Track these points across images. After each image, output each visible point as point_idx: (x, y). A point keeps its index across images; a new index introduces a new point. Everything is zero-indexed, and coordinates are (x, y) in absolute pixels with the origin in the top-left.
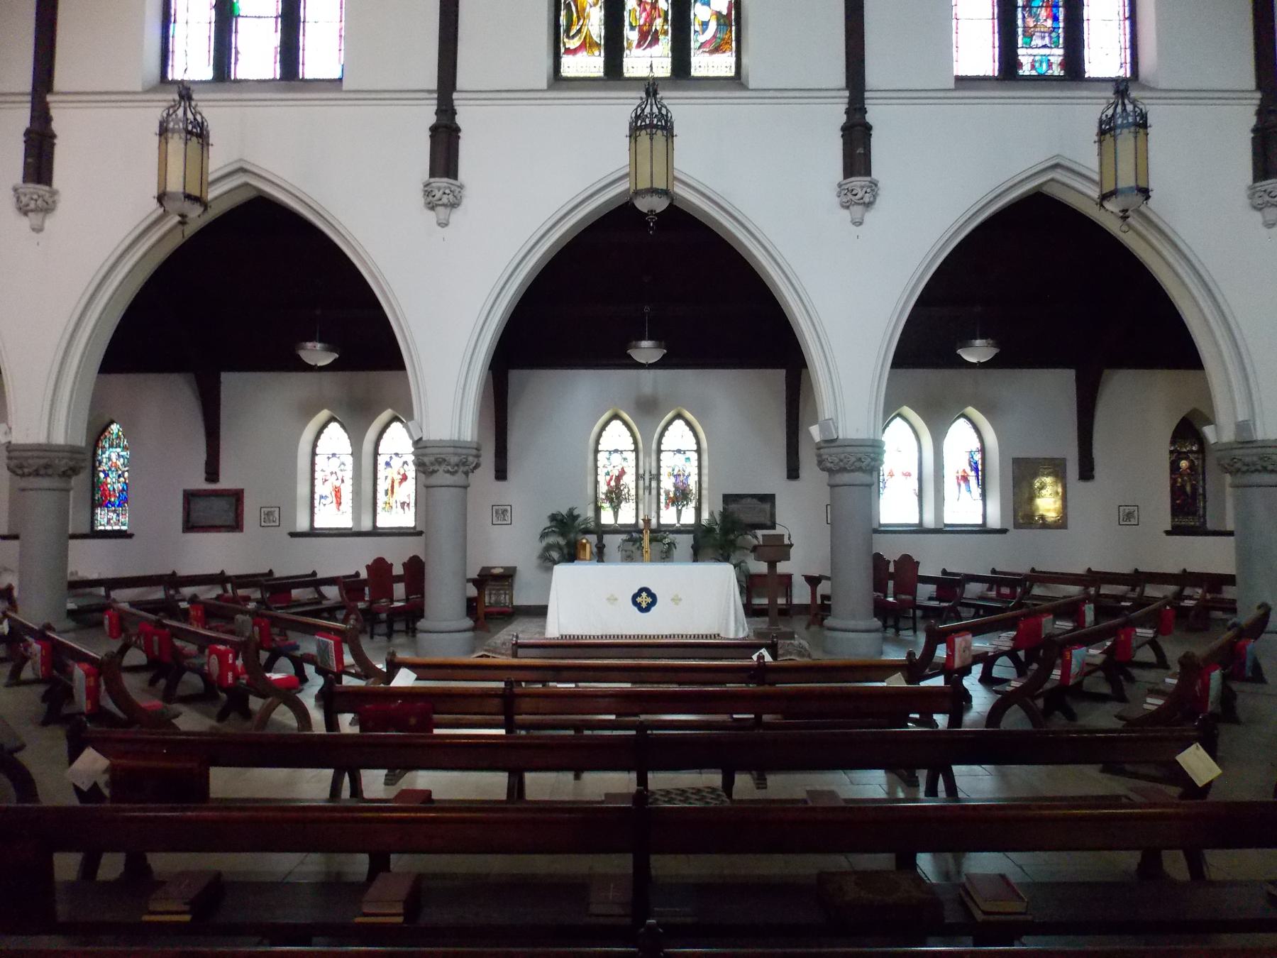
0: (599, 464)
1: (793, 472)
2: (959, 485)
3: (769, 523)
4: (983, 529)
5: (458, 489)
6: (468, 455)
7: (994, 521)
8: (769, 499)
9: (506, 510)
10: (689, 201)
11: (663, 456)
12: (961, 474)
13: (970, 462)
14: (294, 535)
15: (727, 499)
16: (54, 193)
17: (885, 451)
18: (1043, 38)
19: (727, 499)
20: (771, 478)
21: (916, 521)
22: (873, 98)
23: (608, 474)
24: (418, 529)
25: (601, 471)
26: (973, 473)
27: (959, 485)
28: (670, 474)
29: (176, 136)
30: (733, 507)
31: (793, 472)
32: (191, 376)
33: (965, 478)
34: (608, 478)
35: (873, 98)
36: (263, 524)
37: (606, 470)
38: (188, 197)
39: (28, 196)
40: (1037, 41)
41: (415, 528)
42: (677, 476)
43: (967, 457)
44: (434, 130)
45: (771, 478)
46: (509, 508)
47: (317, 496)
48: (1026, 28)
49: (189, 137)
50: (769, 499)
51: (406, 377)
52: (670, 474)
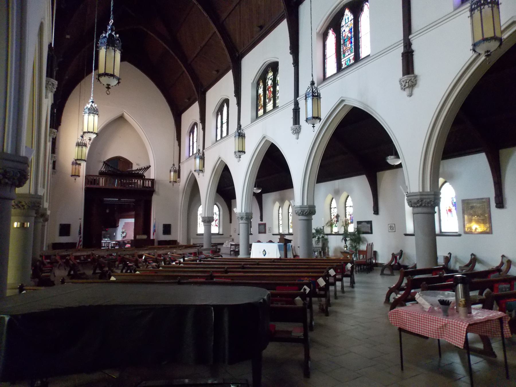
0: (332, 212)
1: (376, 211)
2: (447, 213)
3: (370, 231)
4: (218, 234)
5: (420, 215)
6: (243, 216)
7: (221, 233)
8: (370, 223)
9: (390, 226)
10: (9, 241)
11: (347, 208)
12: (448, 208)
13: (452, 203)
14: (406, 235)
15: (359, 223)
16: (416, 77)
17: (440, 198)
18: (348, 52)
19: (359, 223)
20: (369, 216)
21: (218, 232)
22: (299, 99)
23: (334, 215)
24: (459, 233)
25: (332, 215)
26: (454, 208)
27: (447, 213)
28: (349, 215)
29: (309, 98)
30: (359, 226)
31: (376, 211)
32: (120, 220)
33: (450, 210)
34: (334, 217)
35: (299, 99)
36: (390, 231)
37: (333, 214)
38: (239, 151)
39: (405, 82)
40: (347, 54)
41: (338, 232)
42: (351, 215)
43: (451, 200)
44: (403, 54)
45: (369, 216)
46: (389, 225)
47: (280, 225)
48: (343, 51)
49: (313, 97)
50: (370, 223)
51: (403, 171)
52: (349, 215)
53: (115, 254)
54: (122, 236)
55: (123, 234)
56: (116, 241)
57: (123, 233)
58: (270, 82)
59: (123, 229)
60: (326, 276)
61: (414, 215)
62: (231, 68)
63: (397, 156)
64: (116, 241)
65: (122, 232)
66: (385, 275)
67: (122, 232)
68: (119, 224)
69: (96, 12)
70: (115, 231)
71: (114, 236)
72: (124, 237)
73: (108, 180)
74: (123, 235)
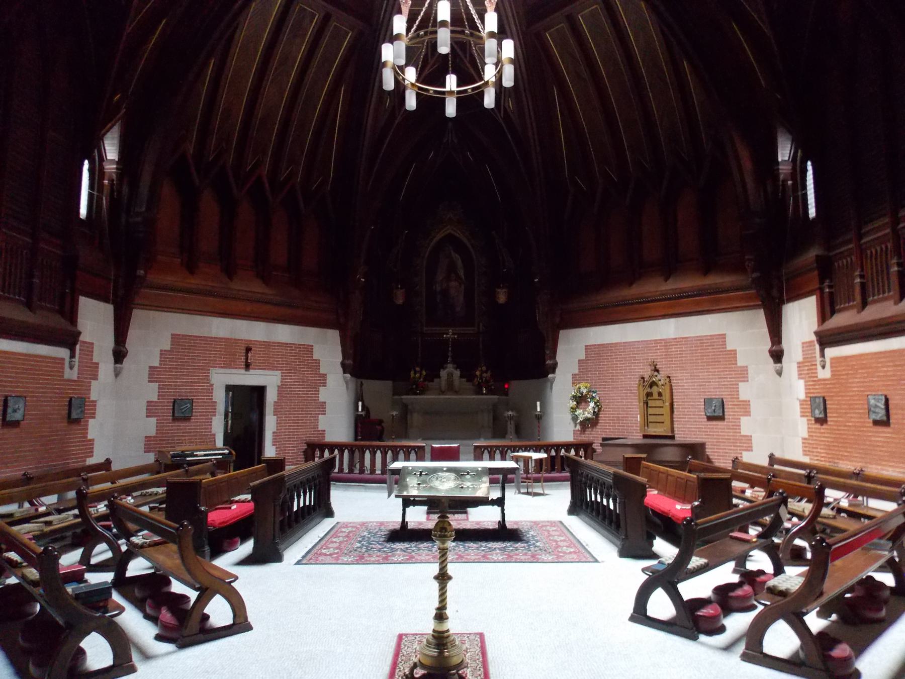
32: (563, 333)
53: (120, 542)
54: (575, 418)
55: (578, 404)
56: (547, 448)
57: (580, 400)
58: (831, 386)
59: (576, 379)
60: (113, 497)
61: (478, 638)
62: (826, 253)
63: (806, 502)
64: (547, 448)
65: (574, 398)
66: (430, 520)
67: (574, 398)
68: (560, 358)
69: (641, 64)
70: (541, 395)
71: (539, 418)
72: (588, 424)
73: (728, 413)
74: (579, 412)
